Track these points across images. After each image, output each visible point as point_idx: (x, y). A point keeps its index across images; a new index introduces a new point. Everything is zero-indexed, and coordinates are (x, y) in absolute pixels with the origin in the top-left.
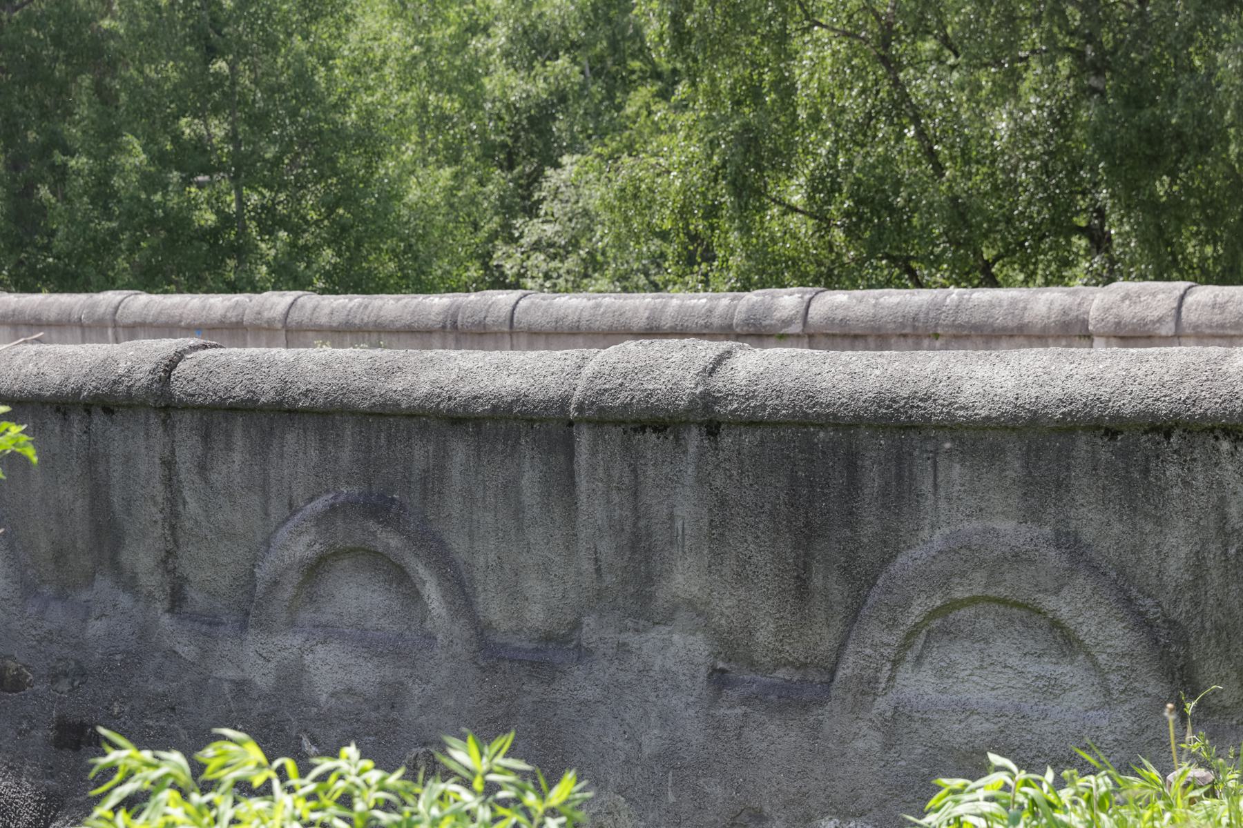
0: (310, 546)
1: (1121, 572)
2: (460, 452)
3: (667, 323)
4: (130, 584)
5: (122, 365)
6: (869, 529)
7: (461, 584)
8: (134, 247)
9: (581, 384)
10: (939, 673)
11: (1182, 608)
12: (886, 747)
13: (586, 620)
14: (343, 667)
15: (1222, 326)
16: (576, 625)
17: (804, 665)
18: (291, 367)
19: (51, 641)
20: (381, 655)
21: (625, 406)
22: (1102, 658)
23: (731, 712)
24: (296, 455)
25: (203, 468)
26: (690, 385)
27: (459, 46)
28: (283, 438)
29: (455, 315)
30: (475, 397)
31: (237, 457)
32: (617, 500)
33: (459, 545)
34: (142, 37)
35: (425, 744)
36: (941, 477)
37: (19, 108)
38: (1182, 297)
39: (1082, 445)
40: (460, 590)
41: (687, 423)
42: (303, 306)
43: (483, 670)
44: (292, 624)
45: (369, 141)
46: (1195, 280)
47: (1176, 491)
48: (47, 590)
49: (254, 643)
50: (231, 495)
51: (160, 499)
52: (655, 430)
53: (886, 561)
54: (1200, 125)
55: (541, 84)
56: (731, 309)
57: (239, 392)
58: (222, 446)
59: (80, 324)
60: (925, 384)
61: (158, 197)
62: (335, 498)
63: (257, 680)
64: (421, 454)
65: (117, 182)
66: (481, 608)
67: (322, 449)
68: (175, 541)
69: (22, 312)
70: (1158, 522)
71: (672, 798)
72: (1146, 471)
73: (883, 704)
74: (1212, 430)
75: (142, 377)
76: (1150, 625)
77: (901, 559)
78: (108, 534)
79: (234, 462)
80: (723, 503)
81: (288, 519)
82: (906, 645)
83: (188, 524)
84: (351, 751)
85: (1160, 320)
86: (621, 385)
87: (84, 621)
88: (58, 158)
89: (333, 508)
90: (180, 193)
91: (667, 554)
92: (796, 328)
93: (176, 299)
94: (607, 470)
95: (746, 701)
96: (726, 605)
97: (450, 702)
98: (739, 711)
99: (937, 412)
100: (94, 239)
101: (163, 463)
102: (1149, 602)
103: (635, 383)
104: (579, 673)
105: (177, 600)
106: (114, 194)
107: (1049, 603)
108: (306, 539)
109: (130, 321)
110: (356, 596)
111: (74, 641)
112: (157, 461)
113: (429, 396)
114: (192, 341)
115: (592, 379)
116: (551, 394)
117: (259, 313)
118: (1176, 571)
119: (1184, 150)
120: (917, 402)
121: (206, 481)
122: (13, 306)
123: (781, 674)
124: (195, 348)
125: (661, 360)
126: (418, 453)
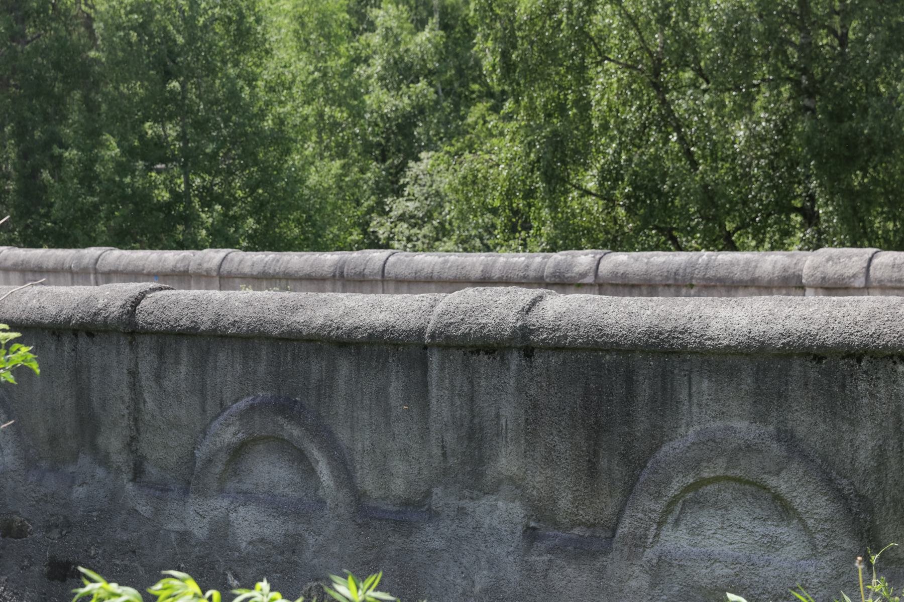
0: (235, 434)
1: (825, 459)
2: (344, 367)
3: (496, 274)
4: (104, 460)
6: (642, 425)
7: (344, 463)
8: (110, 216)
9: (433, 319)
10: (692, 532)
11: (869, 486)
12: (653, 586)
13: (435, 490)
14: (258, 522)
16: (428, 494)
17: (594, 525)
18: (223, 304)
19: (46, 502)
20: (286, 514)
22: (811, 522)
23: (539, 559)
25: (158, 377)
26: (512, 320)
27: (347, 73)
28: (216, 356)
29: (342, 268)
31: (183, 369)
33: (343, 435)
34: (118, 64)
35: (317, 580)
38: (870, 260)
39: (797, 367)
40: (344, 470)
43: (360, 526)
44: (221, 491)
46: (880, 247)
47: (865, 401)
51: (127, 399)
52: (487, 353)
55: (406, 100)
56: (543, 265)
57: (185, 322)
59: (70, 271)
60: (683, 321)
61: (128, 180)
62: (253, 400)
63: (196, 532)
64: (316, 368)
65: (98, 168)
66: (358, 481)
68: (138, 430)
69: (28, 262)
72: (844, 386)
73: (650, 554)
74: (892, 356)
75: (115, 310)
76: (846, 498)
77: (665, 448)
78: (88, 424)
79: (181, 373)
80: (535, 406)
81: (219, 415)
82: (668, 511)
83: (147, 417)
85: (854, 276)
87: (71, 487)
88: (56, 150)
89: (252, 407)
90: (144, 176)
91: (494, 443)
92: (590, 279)
93: (141, 253)
95: (550, 551)
96: (537, 481)
97: (335, 549)
98: (546, 558)
99: (691, 341)
100: (81, 210)
101: (130, 373)
102: (845, 482)
103: (472, 319)
104: (430, 529)
105: (138, 472)
106: (96, 177)
107: (772, 481)
108: (232, 429)
109: (106, 269)
110: (270, 472)
112: (125, 371)
113: (322, 327)
115: (440, 316)
116: (412, 326)
117: (200, 264)
118: (864, 458)
121: (161, 386)
123: (577, 531)
124: (153, 290)
125: (491, 302)
126: (315, 368)
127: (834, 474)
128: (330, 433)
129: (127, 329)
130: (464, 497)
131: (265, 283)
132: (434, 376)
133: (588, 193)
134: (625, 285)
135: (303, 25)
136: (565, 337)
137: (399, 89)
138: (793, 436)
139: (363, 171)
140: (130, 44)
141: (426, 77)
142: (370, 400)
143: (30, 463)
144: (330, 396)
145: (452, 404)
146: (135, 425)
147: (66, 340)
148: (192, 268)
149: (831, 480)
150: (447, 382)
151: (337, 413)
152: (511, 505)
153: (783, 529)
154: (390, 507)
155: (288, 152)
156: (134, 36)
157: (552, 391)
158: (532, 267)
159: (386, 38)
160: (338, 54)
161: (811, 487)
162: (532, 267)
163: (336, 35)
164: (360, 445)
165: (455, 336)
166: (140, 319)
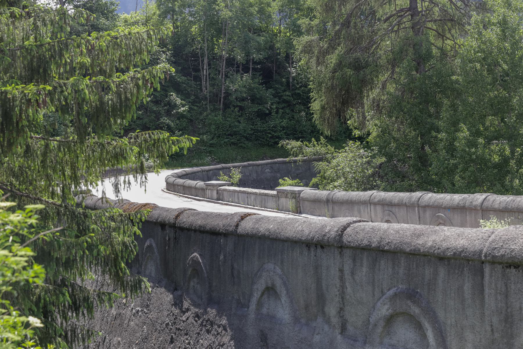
0: (388, 310)
2: (442, 272)
4: (328, 321)
5: (328, 228)
7: (441, 332)
8: (465, 170)
9: (487, 244)
18: (385, 231)
19: (302, 343)
21: (503, 256)
25: (353, 274)
28: (380, 262)
30: (448, 249)
31: (364, 269)
32: (500, 299)
33: (441, 314)
42: (489, 200)
48: (303, 321)
50: (362, 286)
51: (338, 286)
52: (515, 267)
57: (365, 242)
58: (359, 264)
59: (405, 205)
61: (473, 150)
62: (397, 290)
64: (428, 272)
66: (448, 343)
67: (393, 268)
68: (344, 304)
69: (385, 200)
78: (321, 299)
81: (381, 298)
83: (348, 297)
86: (502, 246)
87: (313, 335)
88: (434, 134)
89: (396, 295)
91: (519, 325)
93: (442, 195)
94: (496, 285)
101: (339, 270)
103: (507, 245)
105: (343, 329)
108: (386, 307)
109: (423, 204)
111: (309, 343)
112: (337, 269)
113: (431, 247)
114: (355, 219)
115: (493, 241)
116: (476, 249)
117: (471, 202)
121: (354, 279)
122: (383, 197)
125: (520, 235)
126: (427, 272)
128: (434, 312)
131: (506, 214)
132: (487, 281)
142: (455, 293)
143: (296, 320)
144: (434, 290)
145: (496, 299)
146: (343, 301)
147: (312, 249)
150: (493, 285)
151: (438, 300)
156: (478, 66)
164: (449, 321)
165: (497, 256)
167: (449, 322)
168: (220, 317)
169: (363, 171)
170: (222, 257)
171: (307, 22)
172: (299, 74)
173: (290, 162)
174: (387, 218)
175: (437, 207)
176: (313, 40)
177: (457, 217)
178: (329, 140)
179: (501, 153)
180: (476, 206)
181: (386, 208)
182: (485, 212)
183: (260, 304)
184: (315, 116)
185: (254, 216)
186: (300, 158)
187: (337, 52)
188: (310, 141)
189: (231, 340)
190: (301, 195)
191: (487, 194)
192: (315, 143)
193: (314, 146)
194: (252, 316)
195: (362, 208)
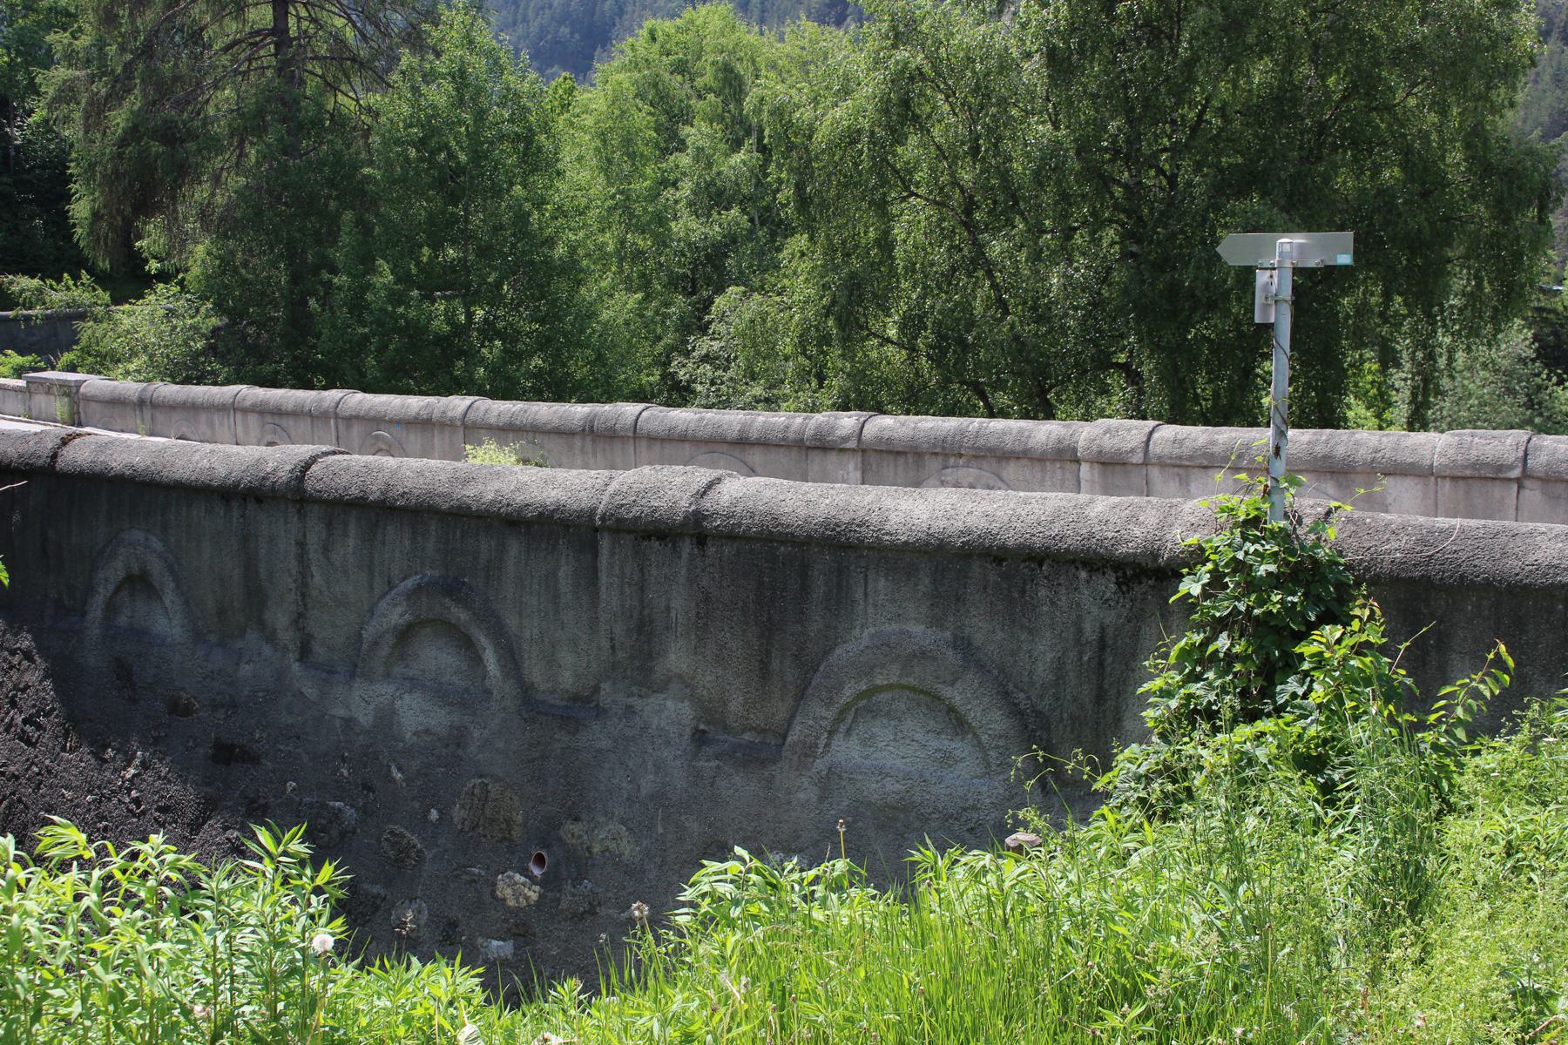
1: (1002, 670)
2: (514, 548)
3: (754, 435)
4: (271, 637)
6: (815, 626)
7: (512, 652)
8: (383, 348)
9: (606, 498)
10: (864, 743)
11: (1046, 701)
12: (821, 799)
13: (603, 685)
14: (423, 712)
15: (1180, 458)
16: (596, 689)
17: (764, 731)
18: (394, 473)
20: (451, 704)
21: (637, 519)
22: (985, 738)
23: (707, 765)
24: (396, 543)
25: (326, 550)
26: (684, 504)
27: (654, 196)
29: (592, 421)
31: (351, 542)
33: (512, 622)
34: (394, 182)
35: (481, 777)
36: (870, 588)
37: (298, 235)
38: (1151, 433)
39: (976, 568)
40: (512, 659)
41: (682, 535)
43: (526, 720)
44: (387, 676)
45: (571, 271)
46: (1159, 417)
47: (1045, 608)
48: (213, 638)
49: (359, 690)
52: (658, 539)
53: (827, 652)
54: (1207, 288)
55: (717, 228)
56: (803, 426)
57: (354, 491)
59: (310, 414)
60: (861, 513)
61: (401, 310)
63: (361, 719)
64: (486, 547)
65: (369, 296)
69: (267, 403)
70: (1031, 631)
71: (660, 830)
72: (1023, 592)
73: (820, 764)
74: (1074, 561)
75: (283, 475)
76: (1022, 713)
77: (838, 651)
78: (256, 597)
79: (349, 545)
80: (707, 600)
82: (839, 719)
83: (315, 593)
84: (156, 839)
85: (1132, 450)
88: (325, 276)
89: (419, 587)
90: (418, 308)
92: (852, 444)
94: (621, 568)
96: (707, 680)
97: (501, 745)
99: (867, 534)
100: (350, 342)
102: (1022, 695)
104: (596, 726)
105: (305, 652)
106: (367, 306)
107: (946, 692)
108: (399, 610)
110: (436, 657)
113: (493, 502)
114: (324, 449)
118: (1043, 671)
119: (1194, 309)
120: (854, 527)
123: (747, 736)
124: (326, 454)
126: (484, 547)
127: (1011, 686)
129: (292, 497)
130: (631, 695)
133: (888, 340)
134: (889, 452)
135: (604, 141)
136: (740, 525)
137: (709, 216)
138: (970, 644)
139: (667, 305)
140: (407, 159)
141: (741, 203)
143: (198, 637)
147: (235, 504)
148: (436, 415)
149: (1007, 695)
152: (680, 705)
153: (957, 744)
154: (558, 702)
155: (579, 283)
156: (413, 153)
157: (725, 584)
158: (792, 429)
159: (696, 159)
160: (643, 176)
161: (986, 700)
162: (792, 429)
163: (642, 155)
166: (310, 485)
167: (527, 634)
168: (16, 635)
169: (186, 343)
170: (16, 518)
171: (66, 41)
172: (30, 141)
173: (16, 320)
174: (269, 438)
175: (376, 420)
176: (78, 78)
177: (414, 439)
178: (102, 279)
179: (450, 319)
180: (452, 420)
181: (269, 418)
182: (472, 430)
183: (111, 608)
184: (79, 230)
185: (91, 438)
186: (37, 311)
187: (126, 104)
188: (59, 280)
189: (45, 678)
190: (82, 390)
191: (472, 398)
192: (71, 283)
193: (68, 289)
194: (94, 631)
195: (216, 418)
